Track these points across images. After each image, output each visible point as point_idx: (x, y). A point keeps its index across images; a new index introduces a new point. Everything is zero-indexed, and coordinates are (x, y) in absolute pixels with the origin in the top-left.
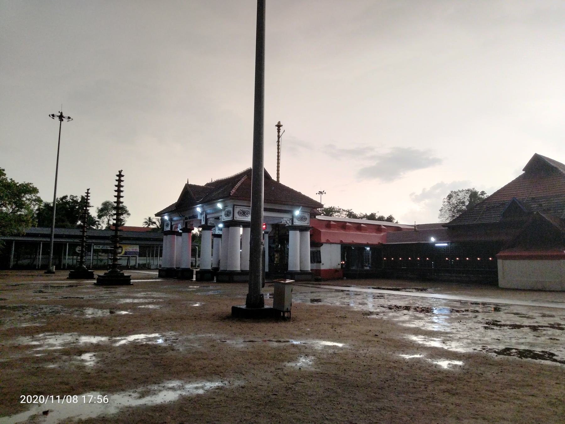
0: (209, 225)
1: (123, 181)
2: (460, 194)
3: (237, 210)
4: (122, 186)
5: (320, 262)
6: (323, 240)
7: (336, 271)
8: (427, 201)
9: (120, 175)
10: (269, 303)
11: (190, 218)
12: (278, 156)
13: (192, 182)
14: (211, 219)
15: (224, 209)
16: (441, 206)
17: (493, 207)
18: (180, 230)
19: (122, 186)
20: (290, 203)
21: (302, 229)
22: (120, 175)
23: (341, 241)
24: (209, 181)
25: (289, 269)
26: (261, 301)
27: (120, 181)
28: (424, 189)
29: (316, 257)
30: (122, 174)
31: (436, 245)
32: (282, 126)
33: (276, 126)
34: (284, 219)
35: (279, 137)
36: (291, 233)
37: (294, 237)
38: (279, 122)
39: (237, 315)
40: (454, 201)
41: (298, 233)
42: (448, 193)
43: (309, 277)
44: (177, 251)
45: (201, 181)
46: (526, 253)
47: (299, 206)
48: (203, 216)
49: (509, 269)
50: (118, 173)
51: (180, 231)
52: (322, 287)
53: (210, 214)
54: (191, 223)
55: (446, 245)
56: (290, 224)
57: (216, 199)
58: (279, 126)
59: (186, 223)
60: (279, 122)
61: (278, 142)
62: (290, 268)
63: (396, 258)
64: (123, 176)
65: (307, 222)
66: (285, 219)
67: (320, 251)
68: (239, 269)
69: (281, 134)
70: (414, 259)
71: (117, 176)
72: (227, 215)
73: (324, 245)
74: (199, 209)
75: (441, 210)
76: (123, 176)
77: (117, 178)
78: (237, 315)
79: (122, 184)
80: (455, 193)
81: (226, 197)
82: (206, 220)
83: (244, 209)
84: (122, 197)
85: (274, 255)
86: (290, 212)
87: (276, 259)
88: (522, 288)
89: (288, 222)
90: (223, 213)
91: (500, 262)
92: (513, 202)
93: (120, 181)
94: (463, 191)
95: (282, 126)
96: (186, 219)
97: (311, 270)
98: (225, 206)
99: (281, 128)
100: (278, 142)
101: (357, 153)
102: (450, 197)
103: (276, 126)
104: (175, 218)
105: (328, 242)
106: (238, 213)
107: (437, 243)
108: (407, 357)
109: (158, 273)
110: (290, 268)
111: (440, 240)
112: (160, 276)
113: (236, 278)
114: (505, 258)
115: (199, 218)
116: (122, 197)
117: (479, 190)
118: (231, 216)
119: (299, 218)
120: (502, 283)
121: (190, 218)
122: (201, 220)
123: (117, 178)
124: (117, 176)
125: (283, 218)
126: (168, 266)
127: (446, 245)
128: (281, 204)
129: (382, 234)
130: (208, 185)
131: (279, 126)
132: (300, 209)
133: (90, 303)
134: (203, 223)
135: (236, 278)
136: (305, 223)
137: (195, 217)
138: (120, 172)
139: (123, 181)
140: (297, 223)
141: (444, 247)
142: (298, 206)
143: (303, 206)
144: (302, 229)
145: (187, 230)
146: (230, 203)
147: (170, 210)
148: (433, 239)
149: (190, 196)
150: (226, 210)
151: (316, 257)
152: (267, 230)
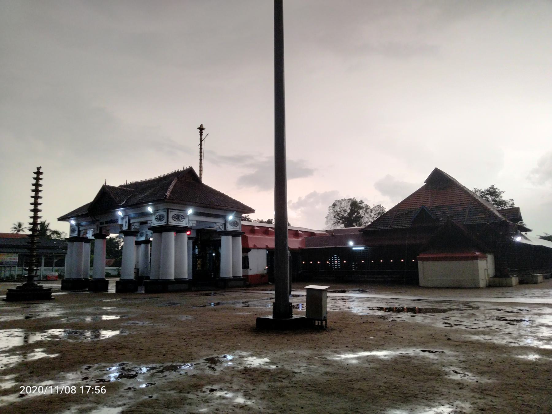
0: (132, 230)
1: (41, 179)
2: (343, 203)
3: (171, 214)
4: (41, 185)
5: (248, 267)
6: (251, 245)
7: (262, 276)
8: (303, 208)
9: (38, 173)
10: (300, 310)
11: (107, 222)
12: (201, 160)
13: (110, 183)
14: (135, 224)
15: (155, 212)
16: (326, 214)
17: (402, 214)
18: (93, 235)
19: (41, 185)
20: (225, 208)
21: (234, 234)
22: (38, 173)
23: (267, 246)
24: (123, 183)
25: (221, 276)
26: (289, 308)
27: (38, 179)
28: (300, 198)
29: (246, 264)
30: (41, 171)
31: (354, 249)
32: (204, 129)
33: (198, 129)
34: (218, 224)
35: (201, 140)
36: (224, 239)
37: (226, 242)
38: (201, 125)
39: (262, 327)
40: (337, 209)
41: (230, 238)
42: (333, 202)
43: (242, 283)
44: (85, 261)
45: (116, 182)
46: (449, 255)
47: (233, 211)
48: (124, 220)
49: (428, 270)
50: (36, 170)
51: (93, 238)
52: (250, 291)
53: (133, 218)
54: (108, 228)
55: (363, 248)
56: (223, 230)
57: (144, 203)
58: (201, 129)
59: (101, 228)
60: (201, 125)
61: (201, 145)
62: (222, 275)
63: (307, 262)
64: (42, 173)
65: (238, 227)
66: (217, 224)
67: (248, 257)
68: (173, 277)
69: (203, 137)
70: (307, 262)
71: (35, 173)
72: (159, 219)
73: (252, 250)
74: (120, 213)
75: (327, 217)
76: (42, 173)
77: (35, 176)
78: (262, 327)
79: (41, 182)
80: (339, 201)
81: (157, 201)
82: (130, 225)
83: (180, 214)
84: (41, 197)
85: (197, 262)
86: (224, 217)
87: (199, 266)
88: (442, 286)
89: (221, 227)
90: (153, 218)
91: (420, 263)
92: (423, 210)
93: (38, 179)
94: (345, 200)
95: (204, 129)
96: (102, 223)
97: (243, 276)
98: (155, 211)
99: (203, 131)
100: (201, 145)
101: (237, 160)
102: (334, 205)
103: (198, 129)
104: (83, 223)
105: (255, 247)
106: (173, 217)
107: (355, 247)
108: (350, 357)
109: (60, 286)
110: (222, 275)
111: (357, 244)
112: (63, 289)
113: (170, 287)
114: (423, 259)
115: (120, 222)
116: (41, 197)
117: (358, 200)
118: (165, 221)
119: (231, 223)
120: (422, 282)
121: (107, 222)
122: (122, 225)
123: (35, 176)
124: (35, 173)
125: (216, 223)
126: (74, 277)
127: (363, 248)
128: (214, 208)
129: (300, 239)
130: (121, 186)
131: (201, 129)
132: (234, 214)
133: (56, 322)
134: (125, 228)
135: (170, 287)
136: (237, 229)
137: (115, 221)
138: (39, 169)
139: (41, 179)
140: (230, 228)
141: (360, 250)
142: (231, 211)
143: (237, 211)
144: (234, 234)
145: (101, 235)
146: (161, 206)
147: (76, 214)
148: (351, 243)
149: (108, 198)
150: (158, 214)
151: (246, 264)
152: (191, 236)
